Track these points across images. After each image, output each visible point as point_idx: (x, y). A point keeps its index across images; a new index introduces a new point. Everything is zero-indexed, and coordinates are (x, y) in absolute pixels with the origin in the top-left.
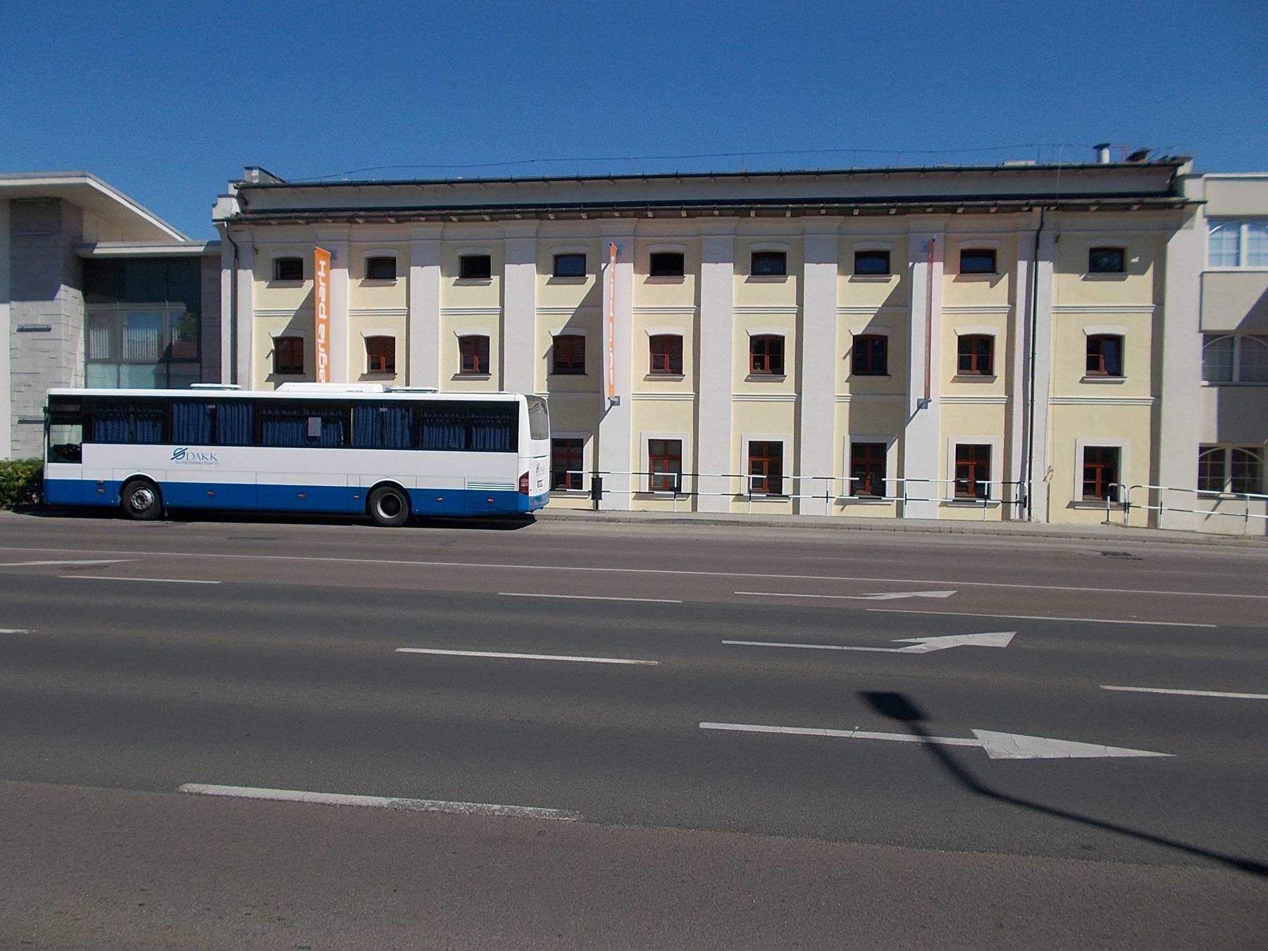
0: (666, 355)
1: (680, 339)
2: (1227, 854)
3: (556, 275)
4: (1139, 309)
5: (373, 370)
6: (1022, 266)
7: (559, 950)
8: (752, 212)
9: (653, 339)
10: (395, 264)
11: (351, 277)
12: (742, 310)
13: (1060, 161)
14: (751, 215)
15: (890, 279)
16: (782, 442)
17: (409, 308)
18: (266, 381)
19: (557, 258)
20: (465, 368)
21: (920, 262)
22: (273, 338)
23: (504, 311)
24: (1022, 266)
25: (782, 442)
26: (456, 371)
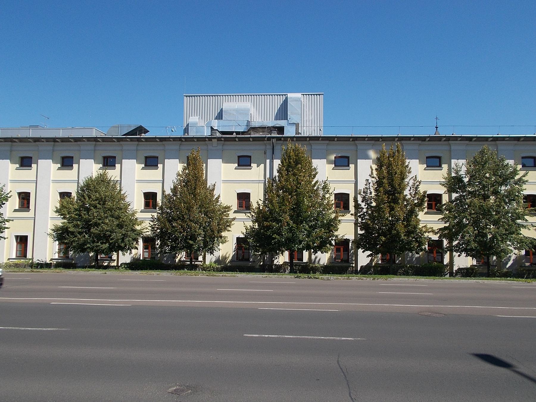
0: (341, 202)
1: (348, 195)
2: (489, 365)
3: (146, 165)
4: (259, 182)
5: (430, 210)
6: (268, 161)
7: (243, 401)
8: (335, 138)
9: (239, 195)
10: (116, 158)
11: (53, 163)
12: (55, 181)
13: (289, 114)
14: (294, 140)
15: (350, 169)
16: (27, 236)
17: (121, 180)
18: (233, 213)
19: (239, 157)
20: (146, 207)
21: (209, 159)
22: (59, 193)
23: (164, 181)
24: (268, 161)
25: (27, 236)
26: (15, 206)
